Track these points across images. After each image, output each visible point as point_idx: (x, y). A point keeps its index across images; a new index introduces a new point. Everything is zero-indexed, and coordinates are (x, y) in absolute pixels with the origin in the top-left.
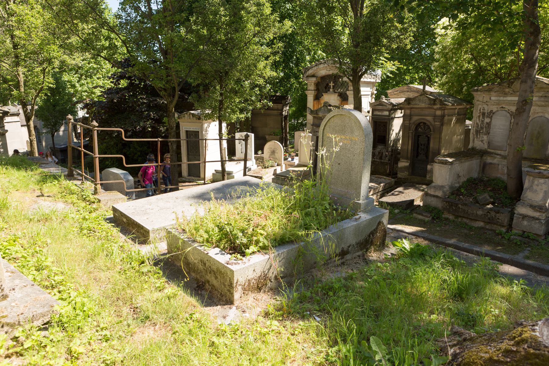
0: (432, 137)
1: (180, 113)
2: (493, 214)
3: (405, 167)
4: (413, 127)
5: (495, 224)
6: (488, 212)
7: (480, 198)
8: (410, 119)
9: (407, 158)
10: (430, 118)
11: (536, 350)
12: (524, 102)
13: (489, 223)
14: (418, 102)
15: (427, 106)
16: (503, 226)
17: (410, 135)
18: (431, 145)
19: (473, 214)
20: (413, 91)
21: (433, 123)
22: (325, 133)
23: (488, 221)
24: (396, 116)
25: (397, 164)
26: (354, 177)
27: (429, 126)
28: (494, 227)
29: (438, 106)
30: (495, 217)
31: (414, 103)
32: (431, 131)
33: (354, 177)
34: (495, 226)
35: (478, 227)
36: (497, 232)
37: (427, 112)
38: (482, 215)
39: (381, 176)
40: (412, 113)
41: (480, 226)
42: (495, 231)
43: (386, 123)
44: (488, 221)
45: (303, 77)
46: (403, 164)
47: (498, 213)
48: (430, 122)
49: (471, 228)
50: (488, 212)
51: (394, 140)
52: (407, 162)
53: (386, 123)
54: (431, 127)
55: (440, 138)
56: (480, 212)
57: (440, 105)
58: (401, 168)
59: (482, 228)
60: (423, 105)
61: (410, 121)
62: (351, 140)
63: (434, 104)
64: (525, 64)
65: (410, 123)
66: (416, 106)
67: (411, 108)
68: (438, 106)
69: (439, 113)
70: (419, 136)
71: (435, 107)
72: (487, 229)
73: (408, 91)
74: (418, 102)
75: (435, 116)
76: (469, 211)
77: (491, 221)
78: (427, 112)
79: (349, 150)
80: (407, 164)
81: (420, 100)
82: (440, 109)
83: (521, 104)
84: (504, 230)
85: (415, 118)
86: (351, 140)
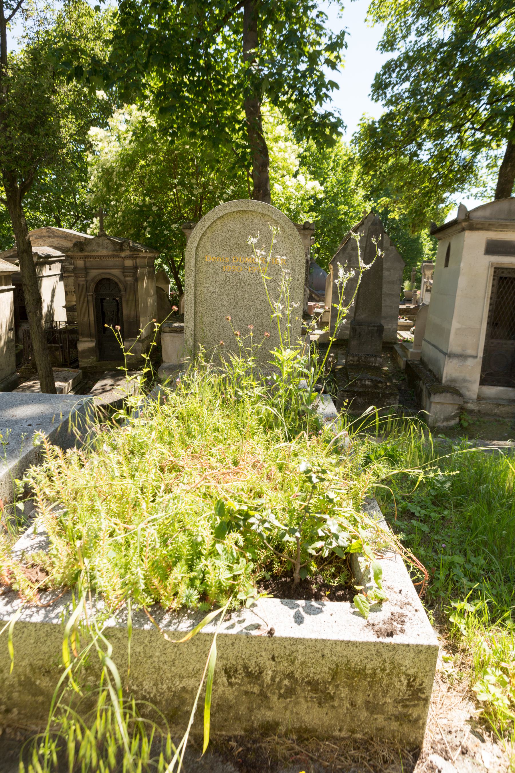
0: (123, 299)
1: (472, 172)
3: (90, 350)
4: (92, 286)
8: (87, 274)
9: (90, 336)
10: (116, 272)
11: (421, 436)
14: (95, 247)
15: (111, 253)
17: (90, 299)
18: (125, 311)
20: (55, 236)
21: (122, 278)
22: (201, 255)
24: (44, 274)
25: (76, 348)
27: (116, 283)
29: (127, 253)
31: (89, 248)
32: (120, 291)
37: (111, 262)
39: (61, 369)
40: (88, 264)
45: (124, 186)
46: (85, 345)
48: (118, 278)
51: (47, 315)
52: (92, 341)
54: (121, 286)
55: (136, 301)
57: (131, 251)
58: (84, 351)
60: (104, 252)
61: (86, 277)
63: (122, 250)
64: (259, 191)
65: (87, 281)
66: (93, 254)
67: (86, 257)
68: (127, 253)
69: (129, 263)
70: (102, 300)
71: (123, 254)
73: (49, 237)
74: (95, 247)
75: (124, 268)
78: (111, 262)
80: (93, 344)
81: (98, 244)
82: (130, 257)
85: (93, 273)
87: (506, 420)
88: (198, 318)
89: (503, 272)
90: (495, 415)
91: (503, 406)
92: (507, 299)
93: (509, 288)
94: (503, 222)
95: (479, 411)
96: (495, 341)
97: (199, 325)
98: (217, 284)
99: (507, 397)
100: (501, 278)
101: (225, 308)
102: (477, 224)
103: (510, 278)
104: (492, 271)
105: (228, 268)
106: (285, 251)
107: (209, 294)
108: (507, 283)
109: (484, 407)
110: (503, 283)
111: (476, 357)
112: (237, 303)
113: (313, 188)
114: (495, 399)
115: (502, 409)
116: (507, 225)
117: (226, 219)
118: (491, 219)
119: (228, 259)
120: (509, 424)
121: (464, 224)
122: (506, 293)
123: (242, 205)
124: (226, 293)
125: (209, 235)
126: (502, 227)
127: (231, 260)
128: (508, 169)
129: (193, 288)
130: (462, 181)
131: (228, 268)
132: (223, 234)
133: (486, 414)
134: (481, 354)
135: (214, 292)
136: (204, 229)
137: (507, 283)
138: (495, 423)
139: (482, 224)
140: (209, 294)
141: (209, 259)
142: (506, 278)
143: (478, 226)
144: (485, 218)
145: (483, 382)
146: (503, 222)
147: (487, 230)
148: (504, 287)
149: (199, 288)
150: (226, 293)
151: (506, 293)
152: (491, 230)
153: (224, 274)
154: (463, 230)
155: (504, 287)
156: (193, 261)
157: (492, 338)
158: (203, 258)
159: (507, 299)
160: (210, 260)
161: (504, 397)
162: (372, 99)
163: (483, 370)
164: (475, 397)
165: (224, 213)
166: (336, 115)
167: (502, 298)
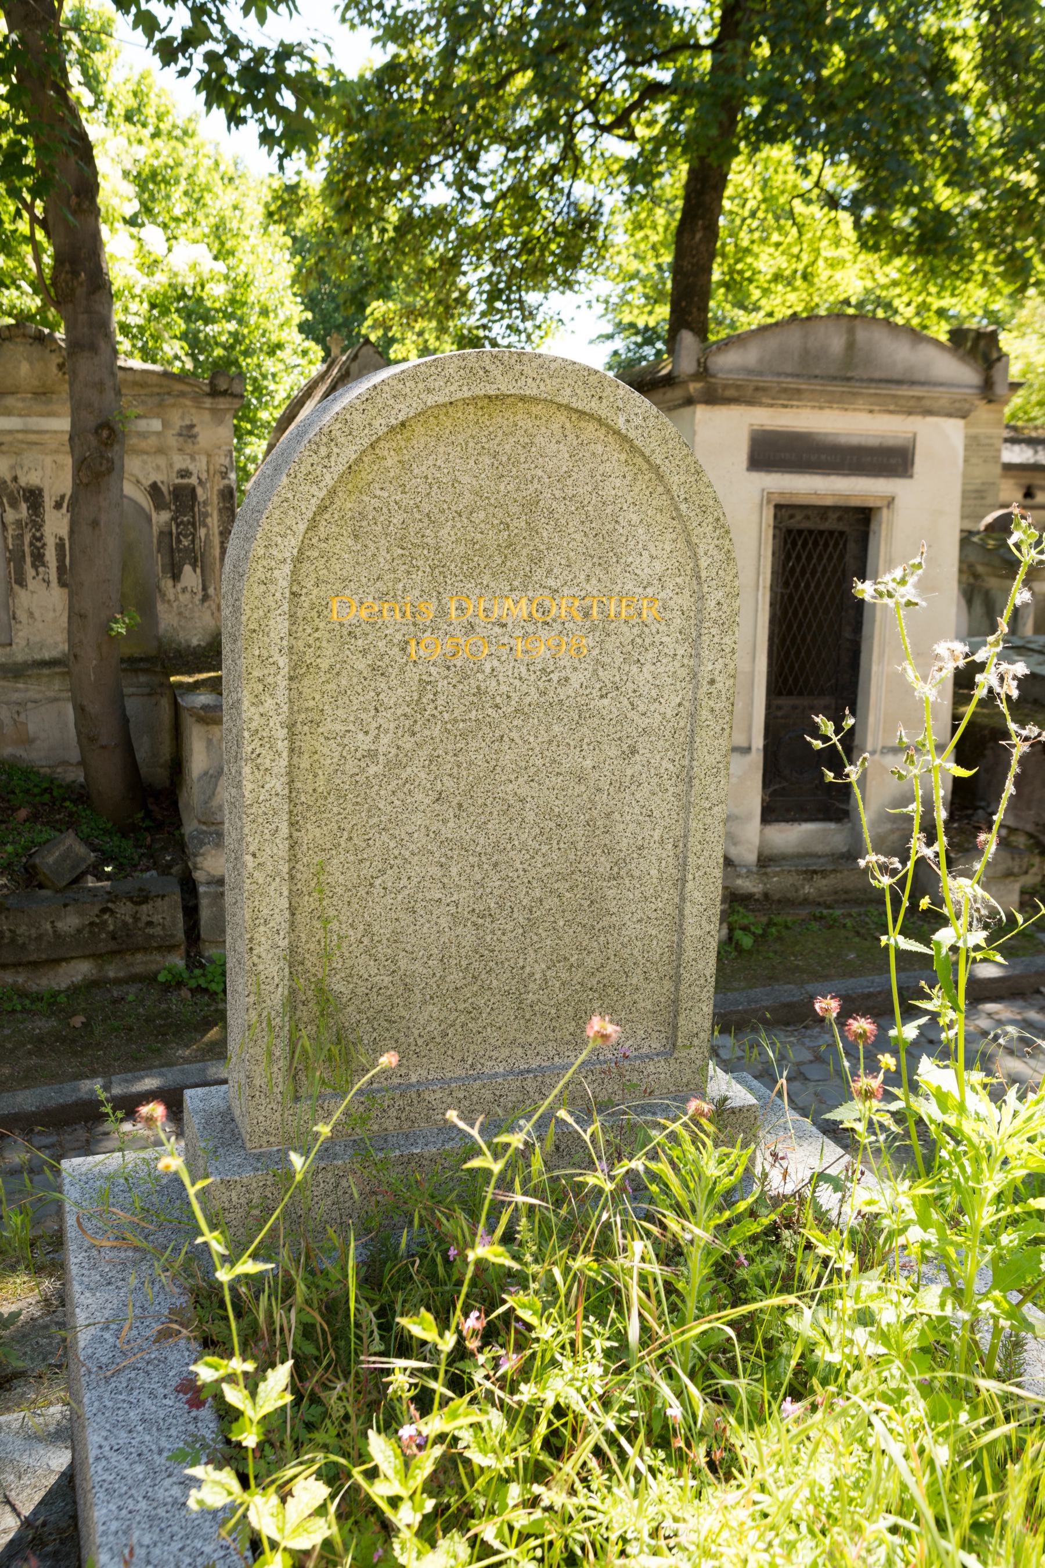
2: (125, 910)
5: (137, 949)
6: (104, 910)
7: (51, 860)
12: (105, 433)
13: (113, 953)
16: (171, 948)
19: (39, 938)
22: (313, 593)
23: (112, 945)
26: (633, 929)
28: (140, 963)
30: (136, 918)
33: (633, 929)
34: (139, 957)
35: (74, 990)
36: (161, 978)
38: (79, 931)
41: (78, 978)
42: (150, 979)
43: (778, 507)
44: (112, 945)
47: (145, 900)
49: (52, 1004)
50: (104, 910)
53: (778, 507)
56: (70, 922)
59: (92, 984)
62: (603, 628)
64: (75, 274)
72: (117, 982)
76: (22, 930)
77: (125, 942)
79: (584, 713)
83: (93, 441)
84: (177, 961)
86: (603, 628)
87: (838, 912)
88: (304, 874)
89: (792, 517)
90: (806, 901)
91: (824, 873)
92: (807, 586)
93: (809, 557)
94: (792, 383)
95: (766, 895)
96: (782, 701)
97: (308, 903)
98: (385, 720)
99: (828, 849)
100: (789, 532)
101: (418, 819)
102: (725, 387)
103: (811, 532)
104: (769, 514)
105: (431, 648)
106: (658, 567)
107: (351, 767)
108: (805, 544)
109: (779, 882)
110: (794, 544)
111: (748, 750)
112: (469, 793)
113: (194, 266)
114: (799, 856)
115: (822, 883)
116: (799, 391)
117: (420, 437)
118: (761, 373)
119: (430, 609)
120: (849, 922)
121: (694, 387)
122: (803, 572)
123: (496, 371)
124: (424, 753)
125: (346, 503)
126: (789, 395)
127: (442, 612)
128: (699, 236)
129: (282, 746)
130: (571, 259)
131: (431, 648)
132: (407, 500)
133: (786, 902)
134: (758, 742)
135: (372, 755)
136: (329, 480)
137: (805, 544)
138: (815, 926)
139: (738, 387)
140: (351, 767)
141: (347, 610)
142: (800, 532)
143: (730, 393)
144: (750, 371)
145: (770, 814)
146: (792, 383)
147: (751, 402)
148: (799, 558)
149: (305, 744)
150: (424, 753)
151: (803, 572)
152: (761, 404)
153: (412, 675)
154: (690, 402)
155: (799, 558)
156: (280, 625)
157: (780, 694)
158: (321, 609)
159: (807, 586)
160: (350, 618)
161: (819, 848)
162: (343, 20)
163: (766, 783)
164: (752, 858)
165: (417, 406)
166: (318, 54)
167: (797, 586)
